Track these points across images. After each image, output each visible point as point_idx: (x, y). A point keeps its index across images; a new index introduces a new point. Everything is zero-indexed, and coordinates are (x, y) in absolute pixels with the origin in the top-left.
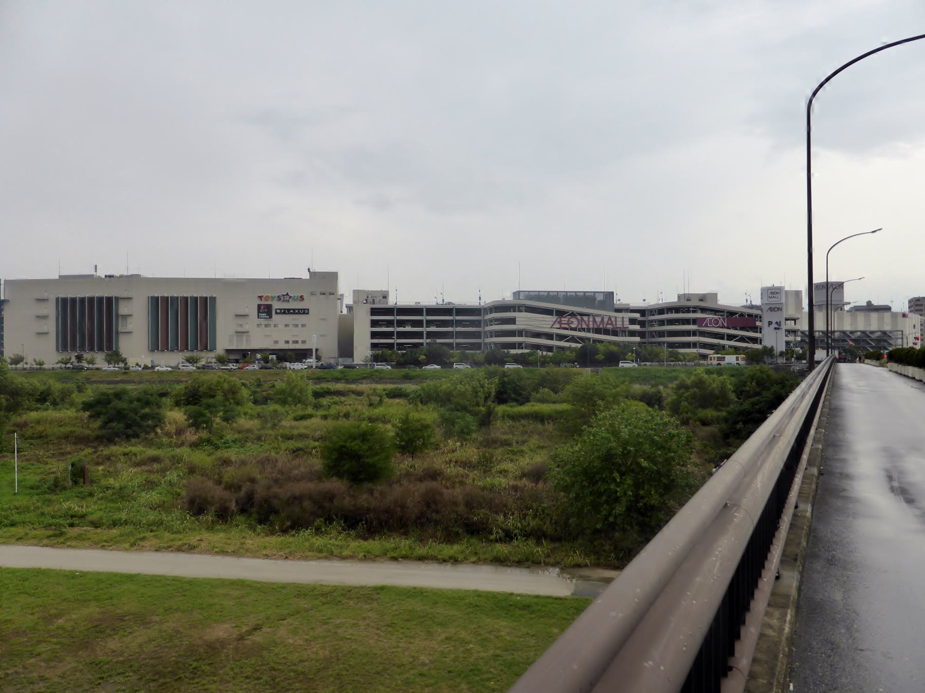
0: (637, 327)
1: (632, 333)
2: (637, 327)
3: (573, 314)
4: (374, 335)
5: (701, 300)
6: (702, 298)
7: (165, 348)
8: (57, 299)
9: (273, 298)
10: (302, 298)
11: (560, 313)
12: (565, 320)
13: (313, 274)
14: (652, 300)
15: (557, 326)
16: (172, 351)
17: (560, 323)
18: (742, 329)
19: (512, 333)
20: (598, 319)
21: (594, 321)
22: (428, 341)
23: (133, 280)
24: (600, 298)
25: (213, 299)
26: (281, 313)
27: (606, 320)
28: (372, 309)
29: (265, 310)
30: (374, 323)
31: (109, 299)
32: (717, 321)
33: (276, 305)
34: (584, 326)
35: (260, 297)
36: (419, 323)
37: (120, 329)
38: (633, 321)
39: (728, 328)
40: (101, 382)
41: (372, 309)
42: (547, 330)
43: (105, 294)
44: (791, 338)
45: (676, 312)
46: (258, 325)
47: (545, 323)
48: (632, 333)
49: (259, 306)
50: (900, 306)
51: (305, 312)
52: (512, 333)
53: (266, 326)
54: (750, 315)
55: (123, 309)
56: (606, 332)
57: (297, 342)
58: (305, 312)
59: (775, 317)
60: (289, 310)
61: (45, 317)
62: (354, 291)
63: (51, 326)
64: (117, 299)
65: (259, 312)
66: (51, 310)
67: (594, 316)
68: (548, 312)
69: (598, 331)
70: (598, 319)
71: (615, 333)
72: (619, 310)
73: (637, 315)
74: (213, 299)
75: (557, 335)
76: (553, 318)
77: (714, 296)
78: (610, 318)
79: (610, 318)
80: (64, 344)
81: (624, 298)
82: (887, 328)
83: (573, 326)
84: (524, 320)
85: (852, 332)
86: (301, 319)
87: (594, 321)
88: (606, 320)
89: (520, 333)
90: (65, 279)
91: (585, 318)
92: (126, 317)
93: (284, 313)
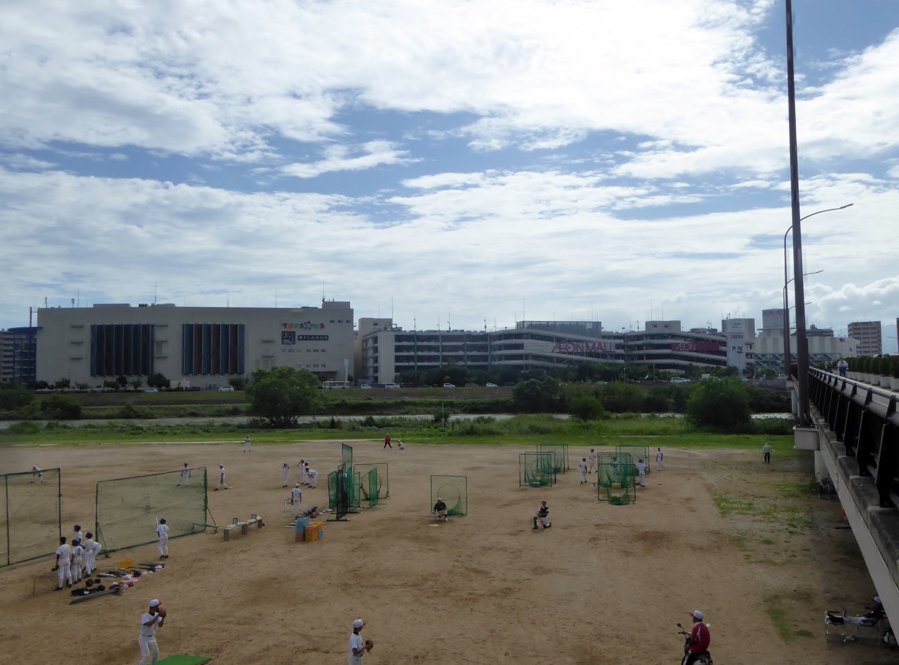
0: (621, 351)
1: (618, 356)
2: (621, 351)
3: (570, 341)
4: (398, 359)
5: (666, 326)
6: (667, 324)
7: (198, 372)
8: (93, 327)
9: (296, 325)
10: (322, 326)
11: (559, 340)
12: (563, 345)
13: (325, 304)
14: (424, 326)
15: (557, 350)
16: (205, 374)
17: (560, 348)
18: (708, 352)
19: (520, 357)
20: (590, 345)
21: (587, 346)
22: (444, 363)
23: (169, 309)
24: (589, 326)
25: (242, 326)
26: (303, 339)
27: (597, 345)
28: (396, 336)
29: (289, 337)
30: (398, 349)
31: (235, 327)
32: (687, 346)
33: (299, 332)
34: (579, 351)
35: (285, 325)
36: (435, 349)
37: (156, 355)
38: (618, 346)
39: (697, 352)
40: (225, 402)
41: (396, 336)
42: (549, 354)
43: (144, 322)
44: (750, 361)
45: (516, 338)
46: (284, 350)
47: (547, 349)
48: (618, 356)
49: (284, 333)
50: (841, 330)
51: (325, 338)
52: (520, 357)
53: (289, 351)
54: (714, 341)
55: (159, 335)
56: (597, 355)
57: (317, 366)
58: (325, 338)
59: (738, 343)
60: (310, 336)
61: (79, 343)
62: (878, 323)
63: (85, 351)
64: (153, 326)
65: (283, 339)
66: (86, 336)
67: (587, 342)
68: (549, 339)
69: (590, 354)
70: (590, 345)
71: (604, 356)
72: (604, 337)
73: (621, 341)
74: (242, 326)
75: (557, 358)
76: (554, 344)
77: (678, 323)
78: (600, 344)
79: (600, 344)
80: (98, 369)
81: (608, 327)
82: (828, 351)
83: (570, 350)
84: (531, 346)
85: (763, 355)
86: (321, 344)
87: (587, 346)
88: (597, 345)
89: (527, 357)
90: (100, 309)
91: (580, 344)
92: (160, 343)
93: (306, 339)
